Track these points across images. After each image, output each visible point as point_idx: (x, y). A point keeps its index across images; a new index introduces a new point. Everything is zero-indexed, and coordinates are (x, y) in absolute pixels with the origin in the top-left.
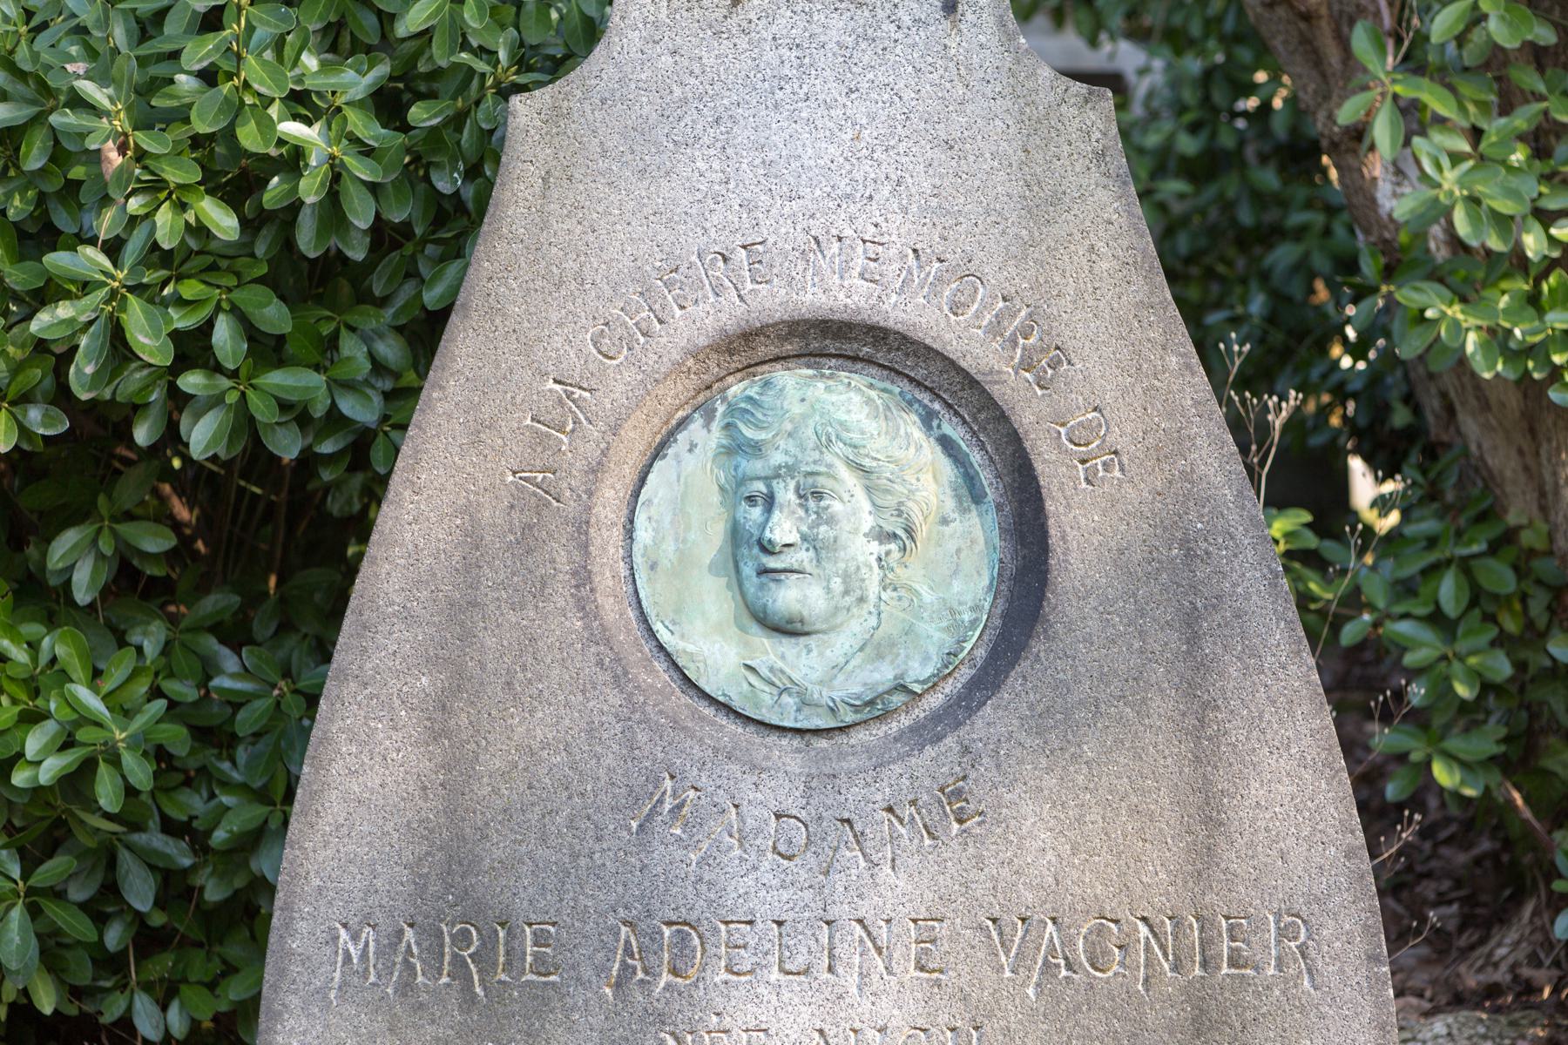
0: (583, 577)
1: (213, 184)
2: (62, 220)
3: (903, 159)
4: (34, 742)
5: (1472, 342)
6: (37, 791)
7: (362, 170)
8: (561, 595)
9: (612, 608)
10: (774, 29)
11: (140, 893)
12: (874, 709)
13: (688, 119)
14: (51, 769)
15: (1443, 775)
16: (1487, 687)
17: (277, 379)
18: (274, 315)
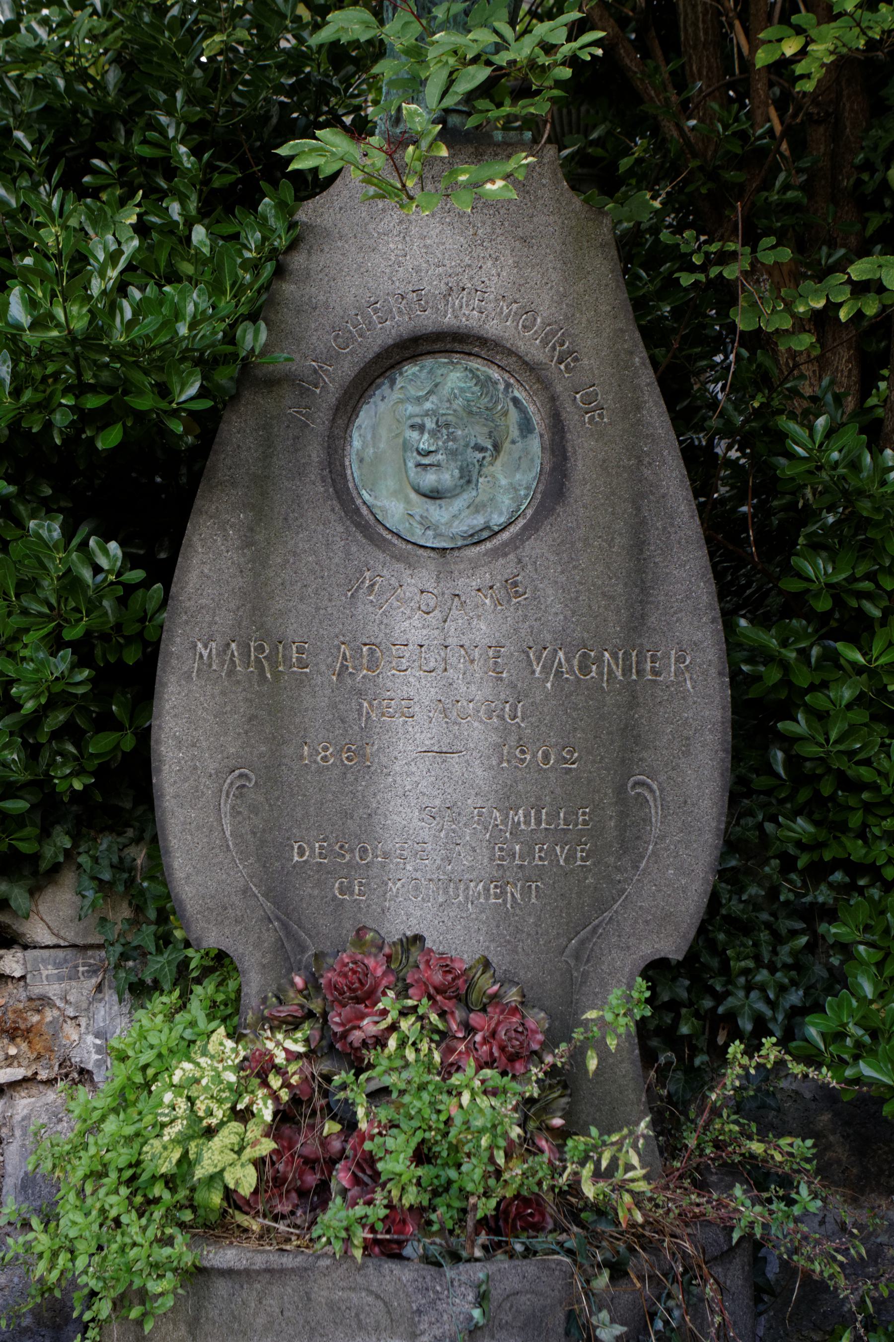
3: (500, 247)
10: (433, 172)
13: (386, 220)
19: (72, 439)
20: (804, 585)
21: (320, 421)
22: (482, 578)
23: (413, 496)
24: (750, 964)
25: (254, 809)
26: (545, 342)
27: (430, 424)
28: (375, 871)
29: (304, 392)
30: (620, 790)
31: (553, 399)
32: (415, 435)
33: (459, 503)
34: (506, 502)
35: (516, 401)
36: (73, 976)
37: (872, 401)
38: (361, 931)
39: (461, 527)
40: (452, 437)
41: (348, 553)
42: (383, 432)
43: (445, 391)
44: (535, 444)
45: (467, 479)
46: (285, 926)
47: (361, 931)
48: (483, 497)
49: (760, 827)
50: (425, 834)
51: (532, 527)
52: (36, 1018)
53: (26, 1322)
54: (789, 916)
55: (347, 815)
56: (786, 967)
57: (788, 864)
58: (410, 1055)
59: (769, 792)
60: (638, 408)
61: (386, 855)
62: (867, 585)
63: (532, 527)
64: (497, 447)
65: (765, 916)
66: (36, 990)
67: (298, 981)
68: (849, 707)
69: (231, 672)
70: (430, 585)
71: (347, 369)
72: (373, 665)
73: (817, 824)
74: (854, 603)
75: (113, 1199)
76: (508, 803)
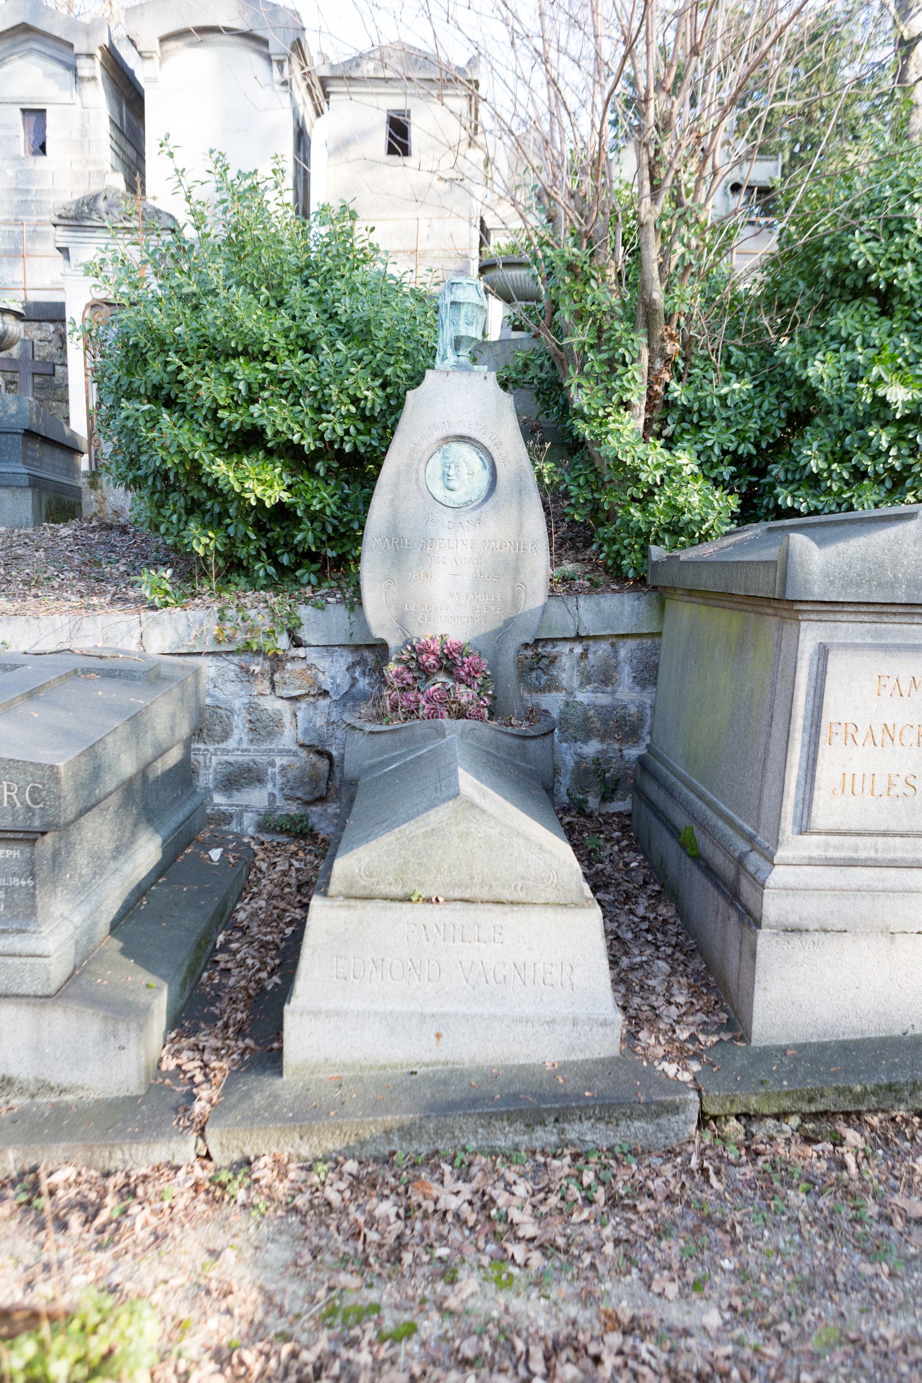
0: (417, 479)
1: (353, 403)
2: (323, 407)
4: (315, 502)
5: (587, 433)
6: (315, 511)
7: (378, 401)
8: (413, 482)
9: (423, 486)
11: (330, 530)
12: (466, 504)
14: (318, 507)
15: (577, 517)
16: (586, 500)
17: (361, 437)
18: (361, 426)
53: (306, 780)
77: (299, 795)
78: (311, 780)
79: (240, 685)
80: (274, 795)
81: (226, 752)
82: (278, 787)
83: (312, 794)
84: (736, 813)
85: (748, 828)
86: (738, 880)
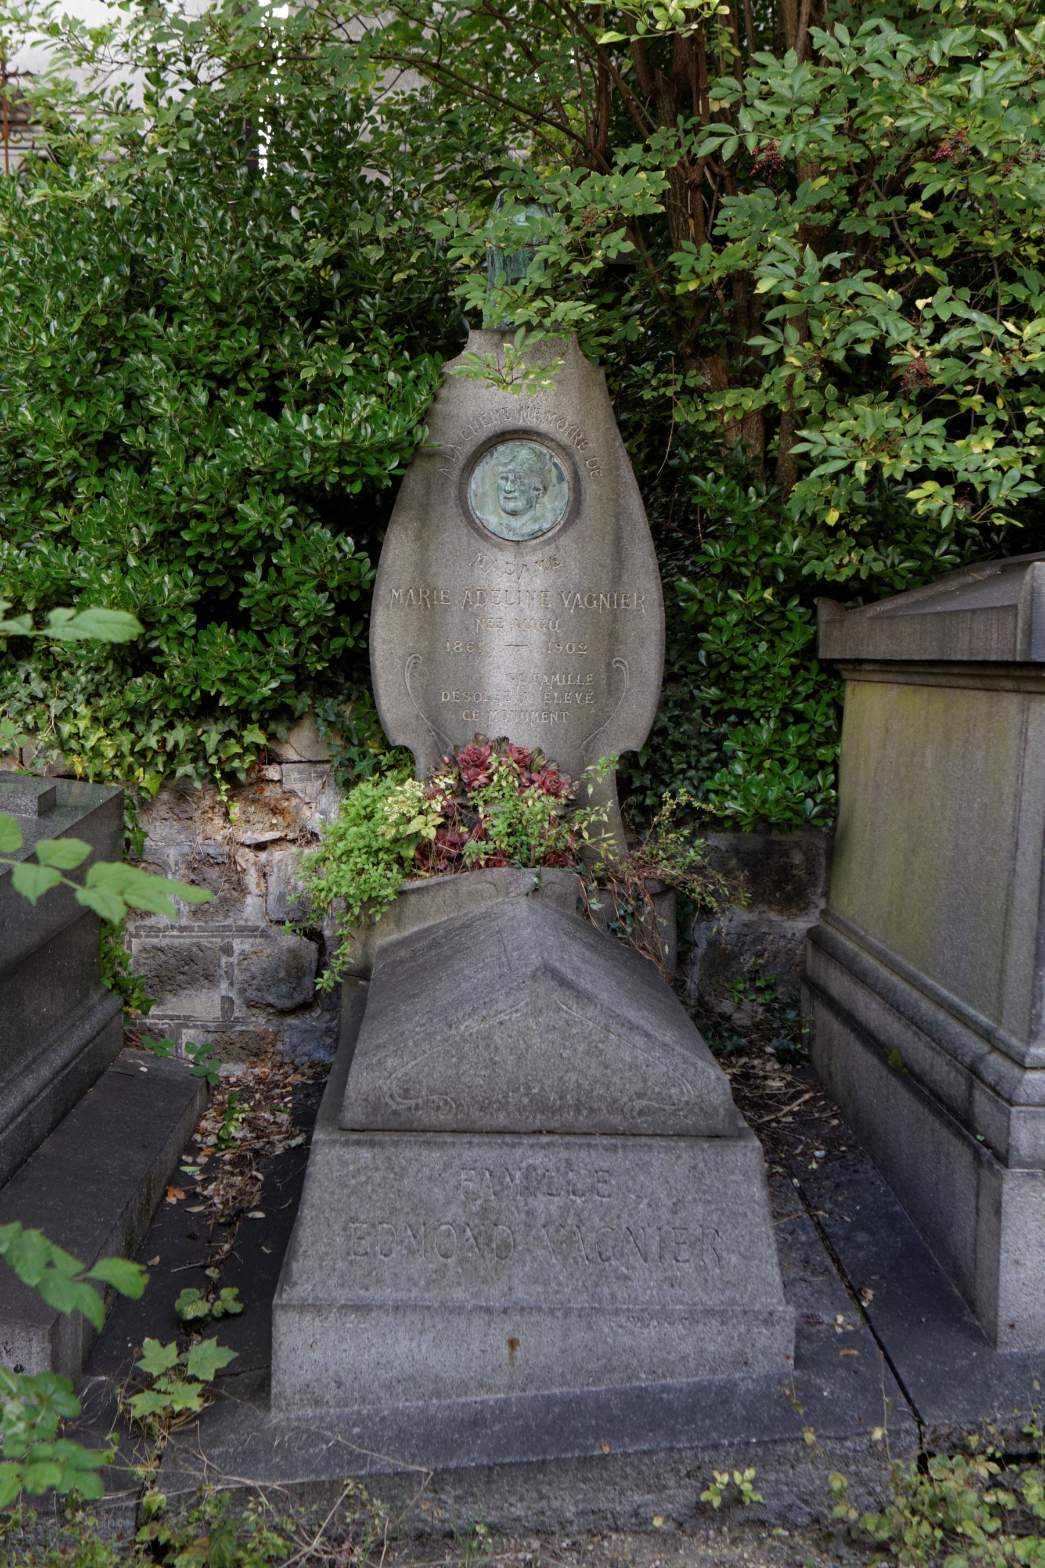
19: (337, 486)
20: (706, 559)
21: (455, 476)
22: (538, 556)
23: (502, 514)
24: (685, 766)
25: (422, 675)
26: (570, 434)
27: (511, 477)
28: (483, 706)
29: (447, 460)
30: (608, 664)
31: (574, 464)
32: (503, 482)
33: (526, 517)
34: (550, 517)
35: (555, 464)
36: (309, 779)
37: (771, 447)
38: (477, 735)
39: (527, 530)
40: (523, 484)
41: (469, 544)
42: (487, 480)
43: (519, 460)
44: (565, 487)
45: (530, 505)
46: (437, 734)
47: (477, 735)
48: (538, 514)
49: (691, 692)
50: (509, 687)
51: (564, 529)
52: (286, 804)
53: (282, 974)
54: (708, 742)
55: (469, 678)
56: (704, 768)
57: (706, 713)
58: (504, 783)
59: (696, 674)
60: (618, 469)
61: (489, 698)
62: (743, 559)
63: (564, 529)
64: (545, 489)
65: (694, 742)
66: (287, 787)
67: (446, 759)
68: (736, 625)
69: (410, 605)
70: (511, 560)
71: (468, 449)
72: (482, 601)
73: (722, 690)
74: (735, 569)
75: (358, 860)
76: (551, 671)
77: (271, 999)
78: (289, 974)
79: (176, 825)
80: (231, 999)
81: (154, 931)
82: (237, 986)
83: (291, 996)
84: (964, 998)
85: (983, 1018)
86: (970, 1099)
